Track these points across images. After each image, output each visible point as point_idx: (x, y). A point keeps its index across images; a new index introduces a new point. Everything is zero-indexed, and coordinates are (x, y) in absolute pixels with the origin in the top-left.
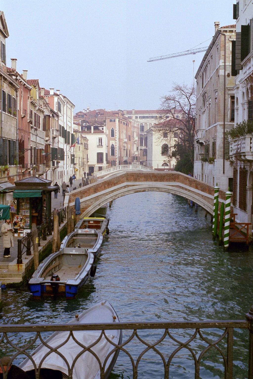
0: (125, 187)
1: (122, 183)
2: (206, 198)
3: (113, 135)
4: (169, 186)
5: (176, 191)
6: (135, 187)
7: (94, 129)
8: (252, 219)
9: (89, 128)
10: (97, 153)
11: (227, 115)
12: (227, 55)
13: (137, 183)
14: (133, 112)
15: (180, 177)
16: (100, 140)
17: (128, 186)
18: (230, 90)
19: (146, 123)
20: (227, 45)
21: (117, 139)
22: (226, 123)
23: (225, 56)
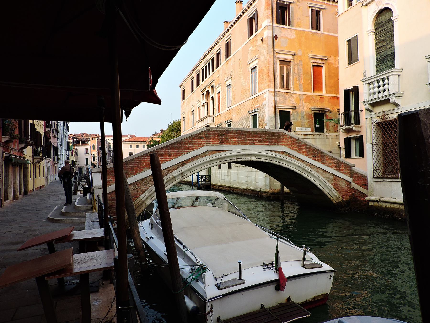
0: (205, 154)
2: (319, 170)
3: (94, 148)
4: (274, 153)
6: (221, 155)
8: (388, 205)
10: (160, 104)
16: (87, 151)
17: (211, 152)
18: (278, 53)
21: (97, 151)
22: (276, 90)
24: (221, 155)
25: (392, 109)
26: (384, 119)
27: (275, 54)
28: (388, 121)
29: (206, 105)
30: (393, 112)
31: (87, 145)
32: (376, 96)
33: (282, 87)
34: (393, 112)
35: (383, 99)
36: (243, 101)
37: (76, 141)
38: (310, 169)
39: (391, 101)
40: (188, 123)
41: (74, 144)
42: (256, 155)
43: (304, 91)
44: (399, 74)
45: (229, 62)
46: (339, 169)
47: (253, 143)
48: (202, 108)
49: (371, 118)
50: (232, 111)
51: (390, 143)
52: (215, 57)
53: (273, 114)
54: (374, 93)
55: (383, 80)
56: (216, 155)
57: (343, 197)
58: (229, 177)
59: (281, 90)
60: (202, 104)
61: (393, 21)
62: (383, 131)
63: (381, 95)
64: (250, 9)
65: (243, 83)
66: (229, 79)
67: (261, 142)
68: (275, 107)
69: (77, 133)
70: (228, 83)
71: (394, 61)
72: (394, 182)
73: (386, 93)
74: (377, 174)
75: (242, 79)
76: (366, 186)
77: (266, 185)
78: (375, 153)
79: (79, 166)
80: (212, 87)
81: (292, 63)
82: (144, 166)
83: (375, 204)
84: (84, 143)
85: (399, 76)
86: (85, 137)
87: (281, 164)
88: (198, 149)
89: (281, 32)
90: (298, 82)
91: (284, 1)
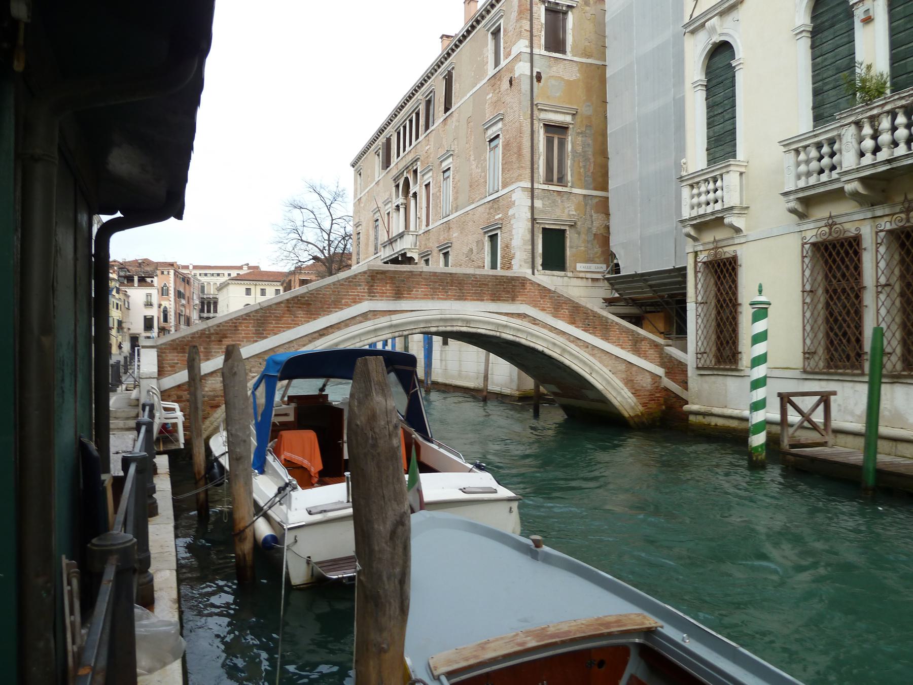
1: (355, 302)
2: (596, 352)
5: (518, 330)
6: (397, 319)
7: (139, 281)
8: (720, 422)
9: (130, 279)
11: (538, 169)
12: (535, 32)
13: (404, 305)
14: (191, 267)
15: (528, 286)
16: (149, 295)
17: (375, 314)
19: (209, 283)
20: (535, 9)
22: (536, 186)
23: (531, 31)
24: (397, 319)
25: (730, 236)
26: (716, 255)
27: (536, 112)
28: (722, 260)
29: (402, 210)
30: (731, 242)
31: (151, 285)
32: (701, 211)
33: (549, 180)
34: (731, 242)
35: (713, 217)
36: (473, 206)
37: (125, 277)
38: (577, 349)
39: (726, 221)
40: (367, 245)
41: (122, 284)
42: (467, 321)
43: (595, 189)
44: (743, 170)
45: (449, 121)
46: (636, 351)
47: (461, 297)
48: (394, 215)
49: (696, 253)
50: (451, 226)
51: (844, 290)
52: (422, 108)
53: (529, 237)
54: (699, 205)
55: (831, 142)
56: (387, 318)
57: (644, 405)
58: (444, 363)
59: (546, 187)
60: (394, 206)
61: (734, 67)
62: (826, 262)
63: (824, 178)
64: (495, 9)
65: (474, 167)
66: (448, 157)
67: (479, 297)
68: (533, 220)
69: (130, 258)
70: (445, 165)
71: (735, 145)
72: (734, 378)
73: (718, 207)
74: (702, 361)
75: (472, 158)
76: (684, 384)
77: (512, 380)
78: (700, 321)
79: (131, 332)
80: (415, 172)
81: (570, 132)
82: (243, 337)
83: (700, 419)
84: (142, 280)
85: (741, 174)
86: (148, 269)
87: (517, 339)
88: (350, 306)
89: (550, 67)
90: (582, 170)
91: (557, 4)
